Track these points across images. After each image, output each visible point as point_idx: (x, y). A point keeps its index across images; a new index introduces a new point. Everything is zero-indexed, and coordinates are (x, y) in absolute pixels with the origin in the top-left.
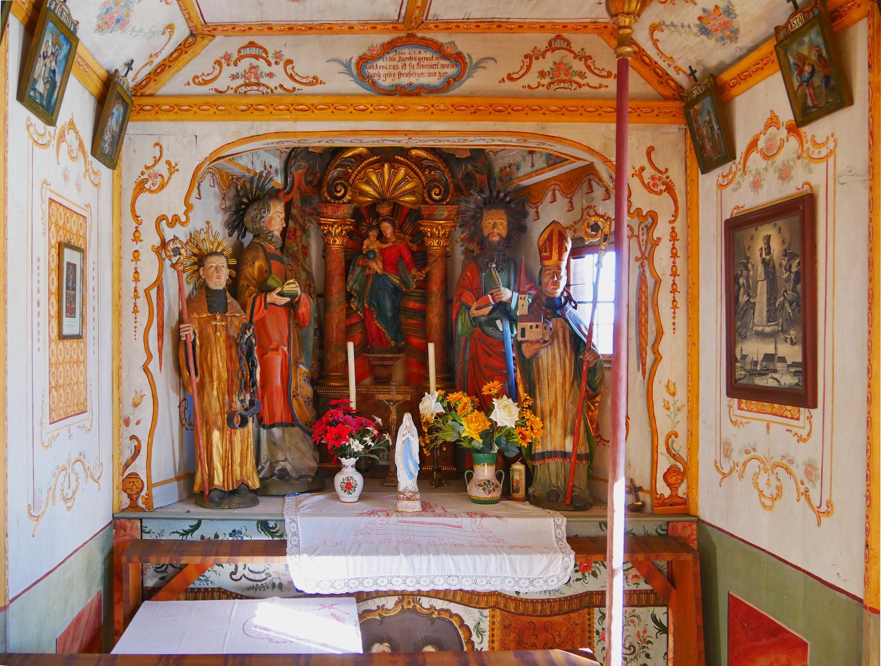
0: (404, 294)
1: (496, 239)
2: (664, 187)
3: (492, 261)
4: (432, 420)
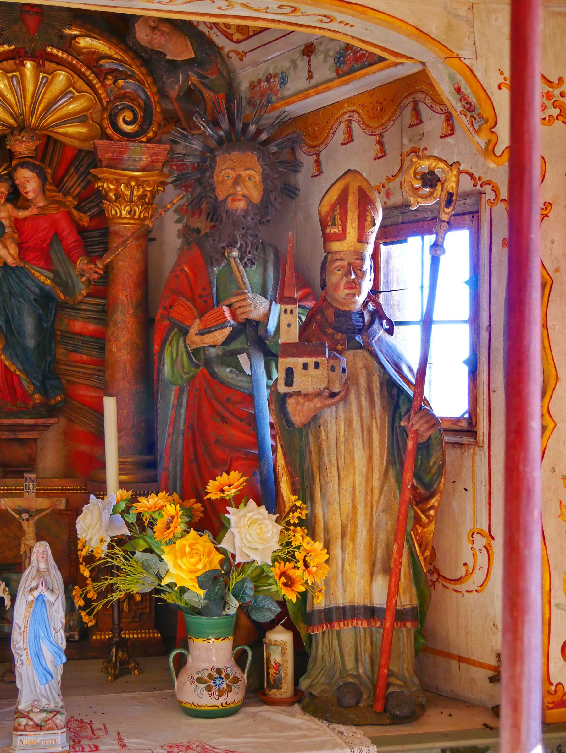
0: (63, 306)
1: (241, 205)
2: (557, 111)
3: (232, 245)
4: (102, 550)
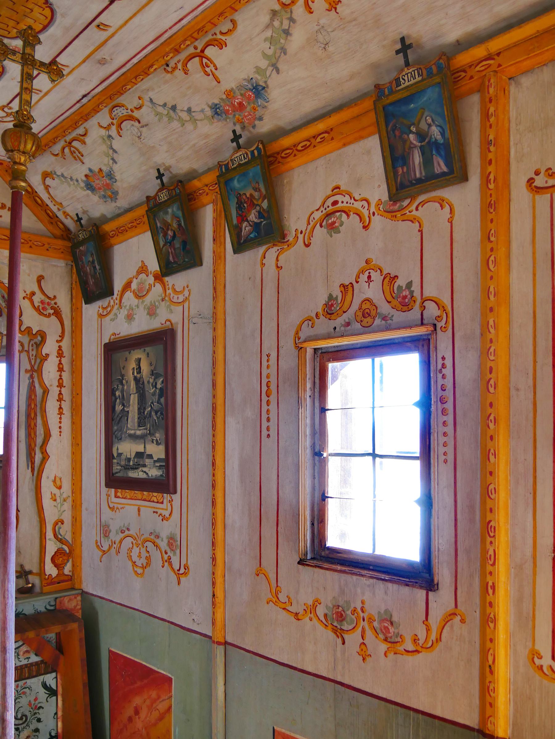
2: (52, 311)
